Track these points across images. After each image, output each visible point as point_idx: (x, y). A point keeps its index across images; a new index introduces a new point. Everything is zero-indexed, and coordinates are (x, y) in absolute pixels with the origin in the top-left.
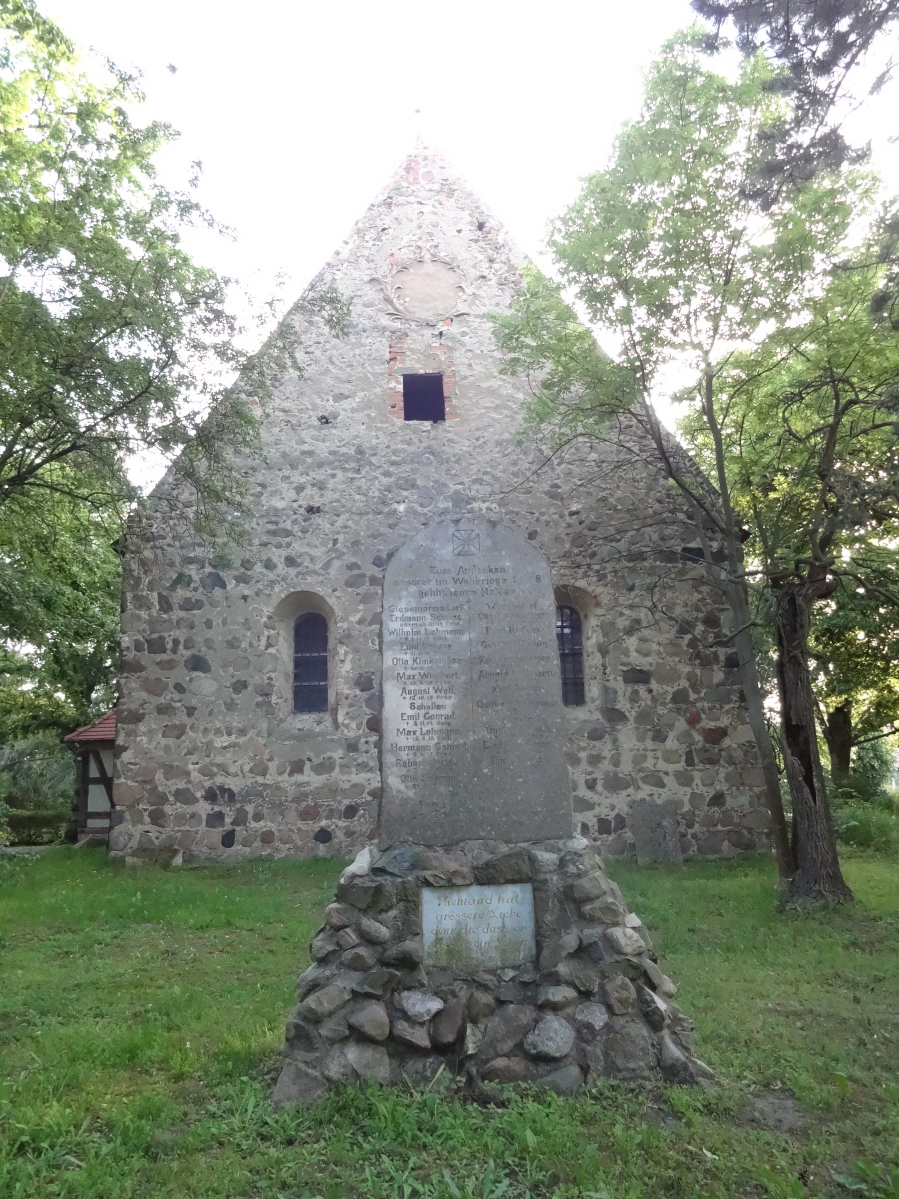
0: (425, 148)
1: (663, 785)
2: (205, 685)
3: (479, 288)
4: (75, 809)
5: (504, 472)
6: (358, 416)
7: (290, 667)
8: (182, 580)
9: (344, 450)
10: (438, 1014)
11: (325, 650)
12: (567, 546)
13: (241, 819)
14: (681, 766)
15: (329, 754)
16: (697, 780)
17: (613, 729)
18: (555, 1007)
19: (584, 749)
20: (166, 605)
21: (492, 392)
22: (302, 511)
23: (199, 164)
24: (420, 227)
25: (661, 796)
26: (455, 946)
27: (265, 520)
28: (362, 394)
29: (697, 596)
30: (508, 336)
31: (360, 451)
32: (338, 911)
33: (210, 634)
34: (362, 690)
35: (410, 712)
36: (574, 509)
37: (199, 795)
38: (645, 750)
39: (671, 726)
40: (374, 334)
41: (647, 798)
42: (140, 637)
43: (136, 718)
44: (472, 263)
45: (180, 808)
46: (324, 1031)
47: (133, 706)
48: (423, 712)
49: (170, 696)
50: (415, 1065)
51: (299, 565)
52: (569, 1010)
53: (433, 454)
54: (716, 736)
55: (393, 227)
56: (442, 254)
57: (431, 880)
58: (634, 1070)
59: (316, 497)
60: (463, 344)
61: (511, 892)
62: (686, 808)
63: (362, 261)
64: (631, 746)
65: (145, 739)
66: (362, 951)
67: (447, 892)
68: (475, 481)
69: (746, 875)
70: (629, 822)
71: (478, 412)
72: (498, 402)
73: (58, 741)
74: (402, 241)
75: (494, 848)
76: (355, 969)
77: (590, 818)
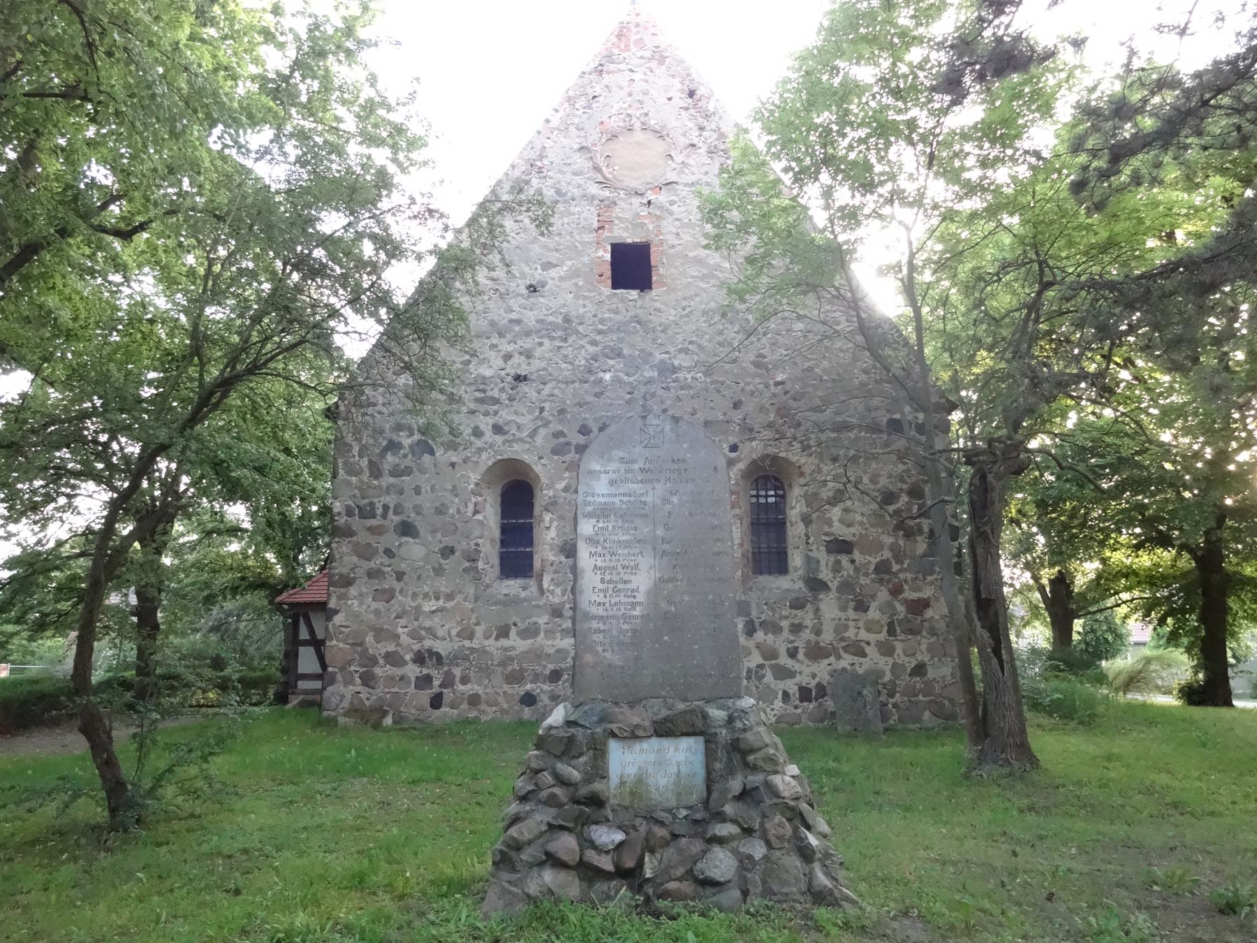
0: (638, 15)
1: (864, 655)
2: (414, 551)
3: (688, 156)
4: (284, 671)
5: (710, 341)
6: (567, 285)
7: (497, 534)
8: (393, 446)
9: (551, 319)
10: (621, 844)
11: (531, 517)
12: (772, 417)
13: (448, 682)
14: (883, 636)
15: (534, 619)
16: (899, 651)
17: (815, 598)
18: (721, 841)
19: (786, 617)
20: (376, 472)
21: (699, 261)
22: (509, 379)
23: (417, 79)
24: (630, 95)
25: (863, 666)
26: (638, 787)
27: (473, 388)
28: (569, 263)
29: (901, 467)
30: (714, 212)
31: (567, 320)
32: (536, 756)
33: (419, 500)
34: (567, 557)
35: (600, 586)
36: (779, 379)
37: (408, 657)
38: (847, 619)
39: (873, 597)
40: (583, 203)
41: (849, 667)
42: (351, 503)
43: (348, 582)
44: (682, 131)
45: (390, 670)
46: (524, 857)
47: (344, 571)
48: (612, 586)
49: (379, 561)
50: (601, 886)
51: (505, 433)
52: (734, 844)
53: (639, 322)
54: (919, 606)
55: (604, 94)
56: (652, 122)
57: (616, 731)
58: (787, 894)
59: (524, 366)
60: (671, 213)
61: (685, 742)
62: (888, 677)
63: (572, 129)
64: (833, 616)
65: (356, 602)
66: (558, 791)
67: (630, 742)
68: (680, 351)
69: (943, 745)
70: (829, 691)
71: (685, 281)
72: (705, 271)
73: (266, 602)
74: (613, 108)
75: (673, 705)
76: (551, 806)
77: (791, 686)
